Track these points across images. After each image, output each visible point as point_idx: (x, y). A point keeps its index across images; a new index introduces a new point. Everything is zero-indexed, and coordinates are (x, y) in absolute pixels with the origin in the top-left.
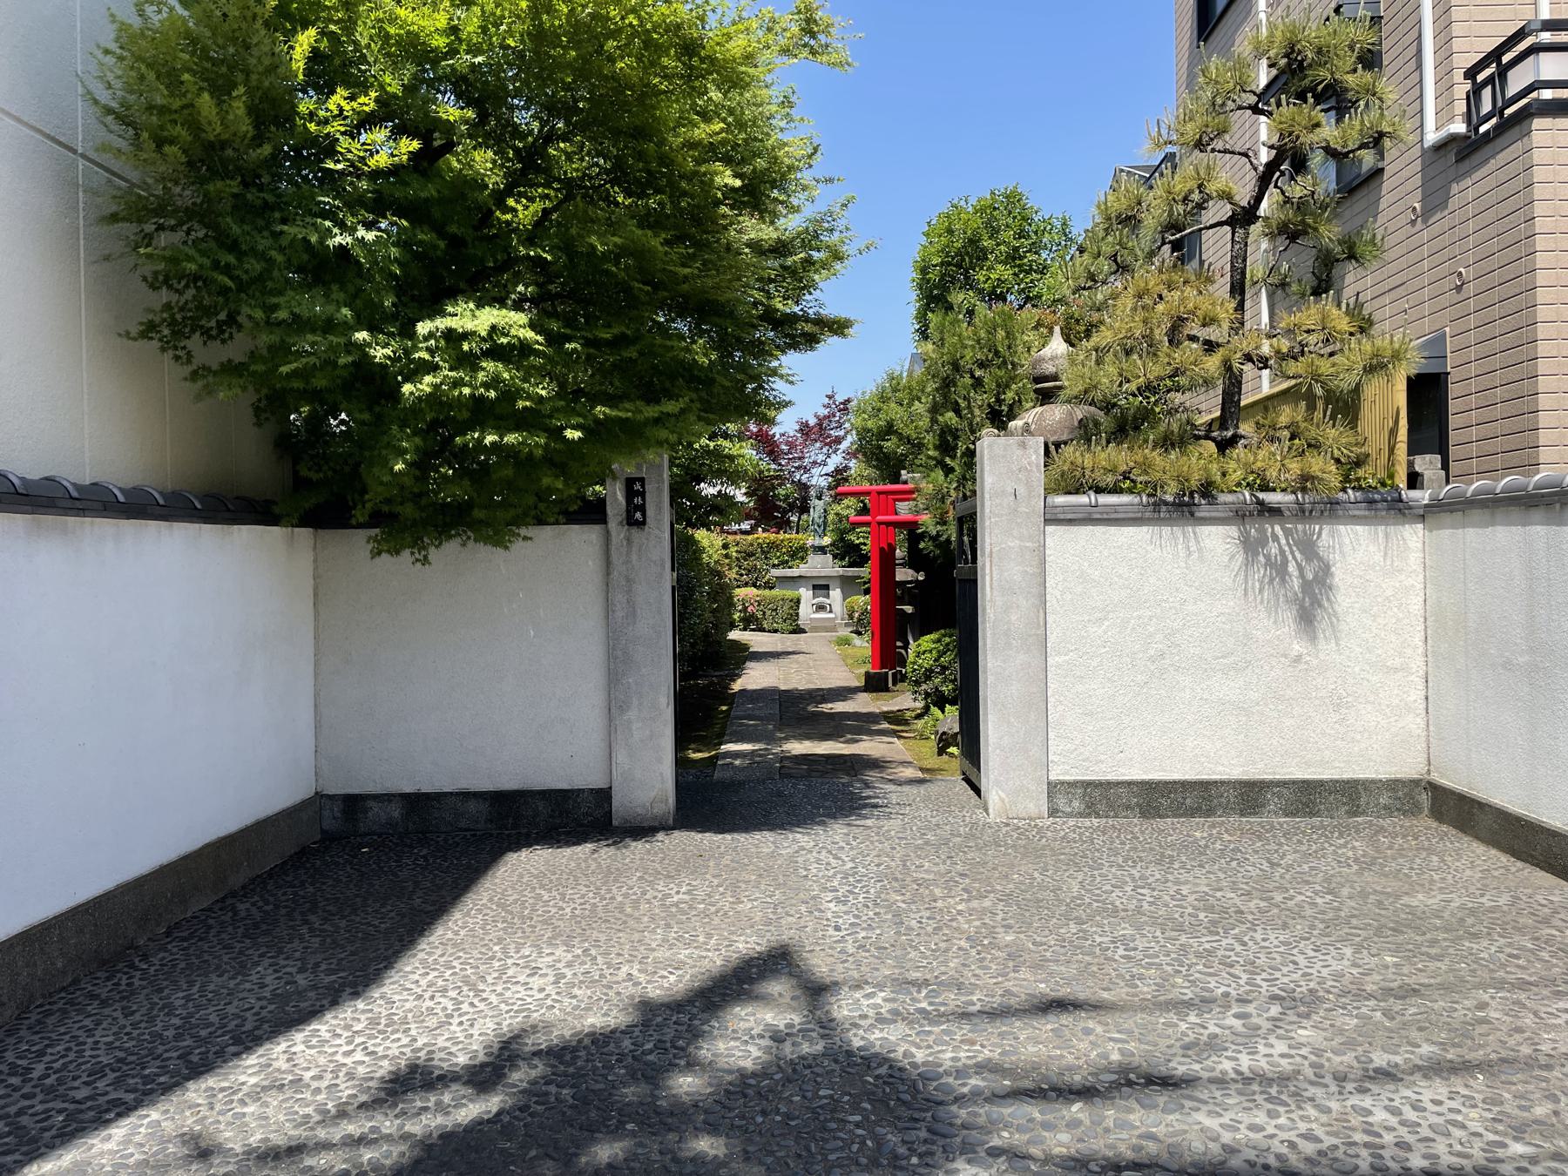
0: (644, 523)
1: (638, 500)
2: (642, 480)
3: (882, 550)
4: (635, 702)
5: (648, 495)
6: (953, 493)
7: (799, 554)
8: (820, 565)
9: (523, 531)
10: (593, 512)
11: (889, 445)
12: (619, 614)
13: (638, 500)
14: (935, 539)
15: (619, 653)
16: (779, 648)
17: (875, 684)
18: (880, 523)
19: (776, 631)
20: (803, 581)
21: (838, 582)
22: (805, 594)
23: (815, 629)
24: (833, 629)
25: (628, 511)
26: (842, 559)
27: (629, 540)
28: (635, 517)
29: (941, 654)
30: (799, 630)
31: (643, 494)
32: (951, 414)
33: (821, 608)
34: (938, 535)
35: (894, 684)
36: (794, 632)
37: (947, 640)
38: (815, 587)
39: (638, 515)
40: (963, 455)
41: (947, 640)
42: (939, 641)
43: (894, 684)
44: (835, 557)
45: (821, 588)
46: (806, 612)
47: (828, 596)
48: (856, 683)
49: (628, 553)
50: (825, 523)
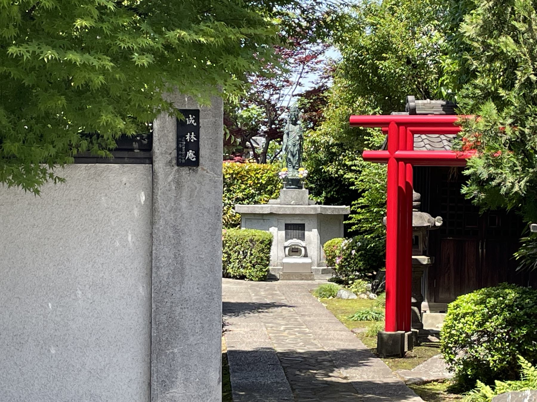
0: (197, 163)
1: (190, 137)
2: (196, 113)
3: (400, 188)
4: (180, 375)
5: (202, 131)
6: (508, 130)
7: (268, 188)
8: (297, 202)
9: (58, 170)
10: (135, 148)
11: (387, 65)
12: (164, 272)
13: (190, 137)
14: (481, 183)
15: (163, 318)
16: (254, 299)
17: (388, 349)
18: (399, 159)
19: (243, 277)
20: (274, 220)
21: (315, 222)
22: (277, 233)
23: (288, 276)
24: (309, 276)
25: (179, 149)
26: (318, 194)
27: (179, 184)
28: (187, 156)
29: (486, 318)
30: (269, 277)
31: (196, 130)
32: (510, 40)
33: (294, 251)
34: (491, 178)
35: (410, 349)
36: (264, 279)
37: (493, 301)
38: (288, 227)
39: (190, 154)
40: (523, 85)
41: (493, 301)
42: (482, 302)
43: (410, 349)
44: (311, 190)
45: (295, 227)
46: (277, 254)
47: (302, 238)
48: (361, 346)
49: (177, 199)
50: (300, 151)
